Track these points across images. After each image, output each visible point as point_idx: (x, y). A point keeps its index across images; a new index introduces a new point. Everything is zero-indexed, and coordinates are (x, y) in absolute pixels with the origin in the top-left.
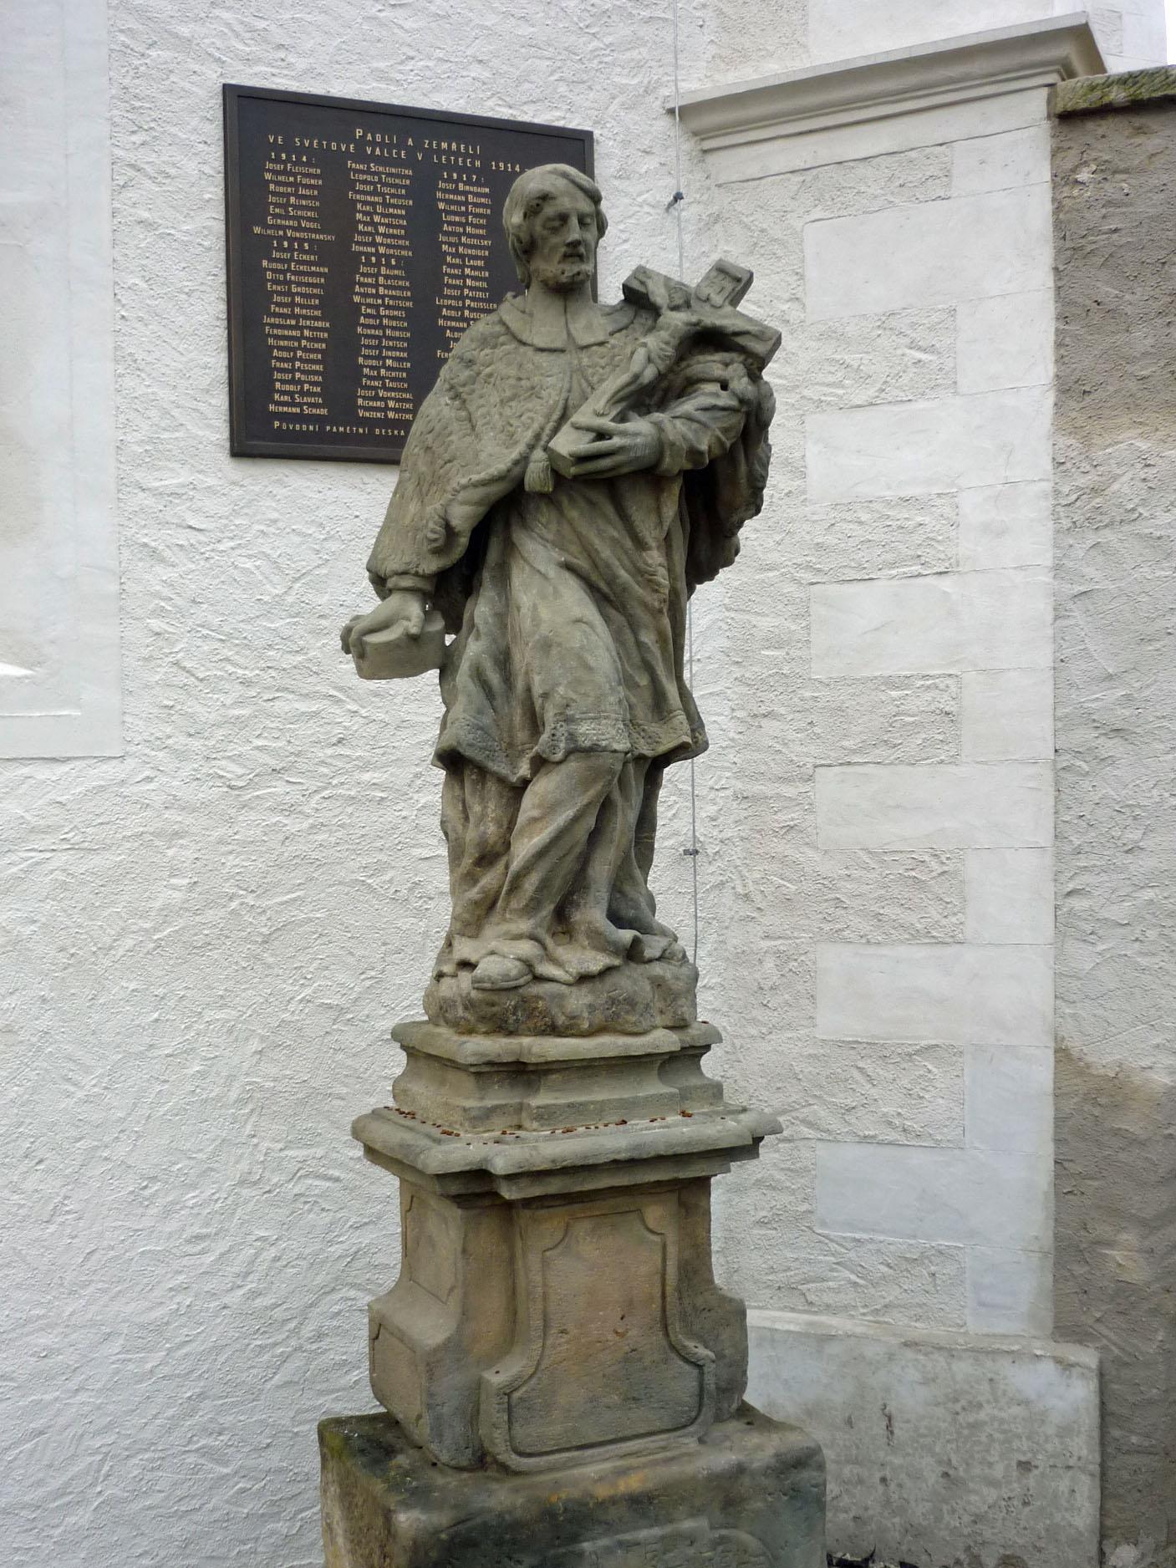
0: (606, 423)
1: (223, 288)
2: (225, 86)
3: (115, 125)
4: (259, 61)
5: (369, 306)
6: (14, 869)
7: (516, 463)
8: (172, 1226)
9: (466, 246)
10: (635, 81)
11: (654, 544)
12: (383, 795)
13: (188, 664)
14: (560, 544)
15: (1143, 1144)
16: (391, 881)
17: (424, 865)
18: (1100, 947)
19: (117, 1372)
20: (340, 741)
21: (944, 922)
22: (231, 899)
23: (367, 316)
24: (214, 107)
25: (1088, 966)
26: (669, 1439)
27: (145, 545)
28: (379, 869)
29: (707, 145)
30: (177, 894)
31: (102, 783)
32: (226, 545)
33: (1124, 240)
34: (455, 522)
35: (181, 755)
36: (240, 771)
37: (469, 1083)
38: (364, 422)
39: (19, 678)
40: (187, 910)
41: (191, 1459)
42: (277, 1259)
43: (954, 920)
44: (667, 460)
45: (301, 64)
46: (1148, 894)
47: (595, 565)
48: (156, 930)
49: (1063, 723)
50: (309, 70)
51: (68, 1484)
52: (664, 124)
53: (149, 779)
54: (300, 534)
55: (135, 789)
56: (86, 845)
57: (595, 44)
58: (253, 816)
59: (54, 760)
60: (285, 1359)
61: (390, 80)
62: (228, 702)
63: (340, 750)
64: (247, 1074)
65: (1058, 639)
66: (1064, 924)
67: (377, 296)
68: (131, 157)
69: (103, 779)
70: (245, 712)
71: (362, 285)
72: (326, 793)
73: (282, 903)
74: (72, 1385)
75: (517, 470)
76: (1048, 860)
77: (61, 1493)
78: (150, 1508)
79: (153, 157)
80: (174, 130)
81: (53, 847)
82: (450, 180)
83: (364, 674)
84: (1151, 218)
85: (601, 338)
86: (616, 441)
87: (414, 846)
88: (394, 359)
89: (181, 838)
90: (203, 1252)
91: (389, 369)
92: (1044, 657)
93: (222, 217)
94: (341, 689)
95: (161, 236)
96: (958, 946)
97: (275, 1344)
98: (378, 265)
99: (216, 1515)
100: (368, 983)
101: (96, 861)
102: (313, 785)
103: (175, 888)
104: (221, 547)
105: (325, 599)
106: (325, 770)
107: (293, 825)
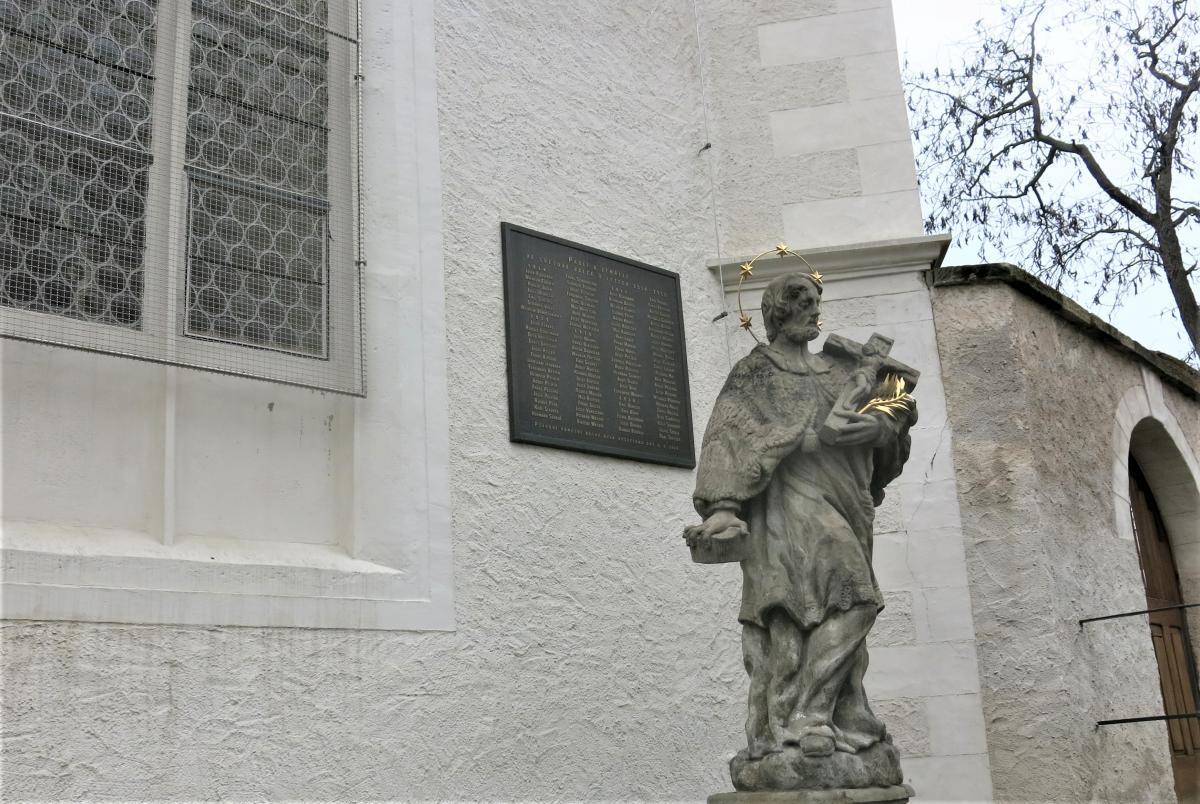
2: (502, 223)
3: (446, 237)
4: (518, 212)
6: (393, 708)
7: (799, 435)
10: (693, 250)
13: (490, 571)
17: (620, 711)
21: (917, 743)
24: (497, 232)
25: (1011, 765)
27: (466, 493)
28: (597, 712)
29: (728, 289)
30: (488, 728)
31: (445, 649)
32: (509, 496)
33: (980, 352)
35: (488, 632)
36: (521, 644)
39: (395, 575)
40: (493, 739)
43: (923, 741)
44: (882, 437)
45: (539, 217)
46: (1043, 719)
47: (840, 497)
49: (978, 619)
50: (543, 221)
52: (707, 275)
53: (470, 648)
54: (548, 493)
55: (463, 654)
56: (434, 692)
57: (674, 227)
59: (416, 632)
61: (581, 233)
62: (514, 598)
63: (573, 633)
65: (971, 568)
68: (455, 258)
69: (444, 646)
72: (566, 661)
73: (547, 735)
75: (799, 439)
76: (978, 700)
79: (466, 258)
80: (476, 245)
82: (615, 291)
83: (696, 559)
84: (996, 341)
87: (615, 698)
88: (593, 391)
89: (489, 688)
92: (962, 580)
93: (502, 297)
95: (471, 305)
96: (927, 759)
100: (594, 792)
101: (440, 703)
102: (560, 655)
103: (487, 724)
104: (506, 497)
105: (562, 535)
107: (552, 681)
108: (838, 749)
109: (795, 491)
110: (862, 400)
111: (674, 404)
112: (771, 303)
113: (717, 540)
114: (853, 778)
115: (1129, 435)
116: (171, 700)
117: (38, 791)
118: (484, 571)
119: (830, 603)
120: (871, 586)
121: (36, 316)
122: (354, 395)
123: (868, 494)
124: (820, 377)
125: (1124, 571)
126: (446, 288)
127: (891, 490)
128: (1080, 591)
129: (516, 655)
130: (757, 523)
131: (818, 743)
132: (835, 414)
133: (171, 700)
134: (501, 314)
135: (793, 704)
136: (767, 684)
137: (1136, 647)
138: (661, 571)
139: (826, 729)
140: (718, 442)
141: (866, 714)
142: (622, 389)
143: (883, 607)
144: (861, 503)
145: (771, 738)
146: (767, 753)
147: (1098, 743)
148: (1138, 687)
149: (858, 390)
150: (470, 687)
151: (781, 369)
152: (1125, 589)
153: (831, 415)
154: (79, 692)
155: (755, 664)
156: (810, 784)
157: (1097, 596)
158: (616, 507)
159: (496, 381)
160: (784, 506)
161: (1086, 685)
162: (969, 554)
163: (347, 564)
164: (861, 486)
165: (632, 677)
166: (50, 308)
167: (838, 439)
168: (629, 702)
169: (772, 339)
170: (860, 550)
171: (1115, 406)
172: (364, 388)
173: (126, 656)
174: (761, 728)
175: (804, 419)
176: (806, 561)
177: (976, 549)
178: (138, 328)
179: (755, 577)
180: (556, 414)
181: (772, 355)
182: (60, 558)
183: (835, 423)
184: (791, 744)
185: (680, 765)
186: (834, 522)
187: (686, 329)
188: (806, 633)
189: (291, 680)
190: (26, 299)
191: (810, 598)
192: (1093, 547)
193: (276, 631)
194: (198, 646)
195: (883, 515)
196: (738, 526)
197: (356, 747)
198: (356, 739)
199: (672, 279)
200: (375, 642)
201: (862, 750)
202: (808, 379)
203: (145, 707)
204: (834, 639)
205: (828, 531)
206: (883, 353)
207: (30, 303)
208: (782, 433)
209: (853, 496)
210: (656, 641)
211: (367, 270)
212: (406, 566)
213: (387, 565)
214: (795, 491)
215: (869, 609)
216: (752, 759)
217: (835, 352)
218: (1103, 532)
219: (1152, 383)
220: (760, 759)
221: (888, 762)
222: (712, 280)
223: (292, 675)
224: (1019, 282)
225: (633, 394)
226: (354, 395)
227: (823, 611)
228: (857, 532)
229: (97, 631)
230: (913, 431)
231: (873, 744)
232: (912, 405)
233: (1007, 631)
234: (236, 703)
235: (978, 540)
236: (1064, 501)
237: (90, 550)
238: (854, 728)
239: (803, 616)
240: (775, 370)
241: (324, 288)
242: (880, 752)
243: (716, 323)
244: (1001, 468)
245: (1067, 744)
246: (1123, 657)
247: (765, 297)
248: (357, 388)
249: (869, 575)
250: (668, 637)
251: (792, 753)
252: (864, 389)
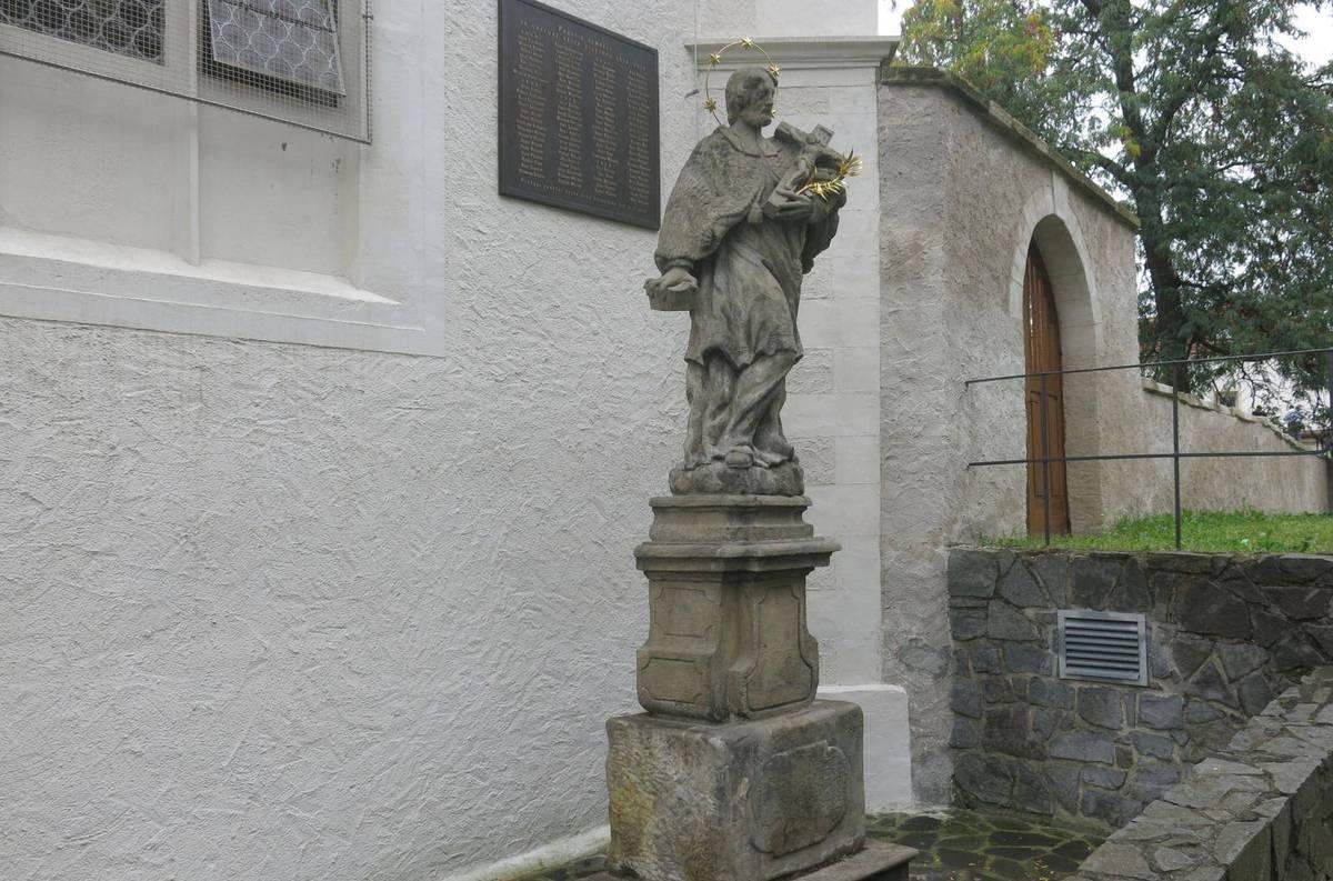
1: (496, 100)
8: (461, 636)
13: (476, 307)
14: (760, 251)
15: (922, 580)
17: (582, 434)
18: (903, 484)
19: (433, 724)
20: (546, 360)
22: (495, 445)
25: (897, 493)
28: (564, 433)
29: (702, 68)
34: (717, 234)
36: (501, 372)
37: (723, 517)
38: (561, 186)
41: (469, 777)
42: (512, 656)
44: (814, 215)
46: (926, 458)
47: (775, 264)
48: (460, 459)
49: (885, 375)
51: (407, 795)
52: (684, 53)
53: (458, 372)
54: (530, 243)
58: (506, 398)
60: (515, 715)
63: (546, 365)
64: (500, 547)
65: (883, 333)
66: (885, 475)
70: (505, 339)
72: (540, 389)
74: (411, 733)
77: (403, 800)
78: (449, 808)
79: (464, 20)
83: (653, 307)
85: (775, 153)
86: (798, 203)
90: (477, 652)
92: (875, 341)
93: (496, 60)
94: (547, 332)
97: (511, 707)
99: (481, 812)
101: (431, 416)
103: (469, 436)
106: (539, 376)
107: (526, 405)
108: (755, 464)
109: (739, 255)
110: (800, 183)
111: (645, 172)
112: (733, 90)
113: (672, 292)
114: (765, 486)
115: (1032, 228)
116: (201, 399)
117: (92, 467)
118: (472, 307)
119: (759, 348)
120: (793, 337)
121: (120, 59)
122: (359, 141)
123: (798, 263)
124: (768, 159)
125: (1009, 344)
126: (446, 47)
127: (820, 259)
128: (970, 358)
129: (497, 381)
130: (706, 281)
131: (739, 458)
132: (778, 192)
133: (201, 399)
134: (495, 76)
135: (722, 428)
136: (703, 411)
137: (1011, 408)
139: (746, 448)
140: (679, 209)
141: (780, 439)
142: (600, 154)
143: (802, 356)
144: (792, 269)
145: (703, 454)
146: (698, 465)
147: (967, 481)
148: (1007, 439)
149: (798, 173)
150: (456, 405)
151: (737, 150)
152: (1009, 359)
153: (774, 192)
154: (122, 387)
155: (695, 395)
156: (730, 489)
157: (984, 363)
158: (588, 260)
159: (487, 138)
160: (728, 267)
161: (964, 434)
162: (883, 320)
163: (352, 294)
164: (793, 255)
165: (594, 406)
166: (43, 27)
167: (778, 214)
169: (732, 122)
170: (786, 307)
171: (1024, 203)
172: (370, 136)
173: (164, 359)
174: (696, 447)
175: (752, 194)
176: (743, 313)
177: (890, 316)
178: (160, 62)
179: (701, 325)
180: (644, 200)
181: (730, 137)
182: (101, 270)
183: (777, 200)
184: (718, 458)
185: (630, 481)
186: (769, 282)
187: (661, 101)
188: (737, 372)
189: (304, 389)
190: (123, 45)
191: (743, 344)
192: (986, 322)
193: (291, 346)
194: (226, 356)
195: (808, 281)
196: (689, 281)
197: (359, 448)
198: (359, 442)
199: (651, 55)
200: (376, 361)
201: (773, 466)
202: (760, 161)
203: (178, 403)
204: (760, 377)
205: (762, 291)
207: (24, 20)
208: (733, 205)
209: (786, 262)
210: (615, 377)
211: (372, 24)
212: (403, 298)
213: (386, 296)
214: (739, 255)
215: (792, 356)
216: (687, 470)
217: (784, 138)
218: (997, 310)
219: (1060, 188)
220: (693, 469)
221: (793, 476)
222: (687, 58)
223: (305, 385)
224: (953, 87)
226: (359, 141)
227: (753, 355)
228: (787, 294)
229: (136, 336)
230: (841, 212)
231: (782, 463)
232: (842, 191)
233: (906, 387)
235: (892, 310)
236: (967, 281)
237: (126, 265)
238: (769, 449)
239: (736, 358)
240: (732, 151)
241: (335, 36)
242: (787, 468)
243: (688, 99)
244: (916, 248)
245: (941, 478)
246: (998, 414)
247: (730, 83)
248: (363, 136)
249: (792, 328)
250: (625, 374)
251: (719, 466)
252: (804, 173)
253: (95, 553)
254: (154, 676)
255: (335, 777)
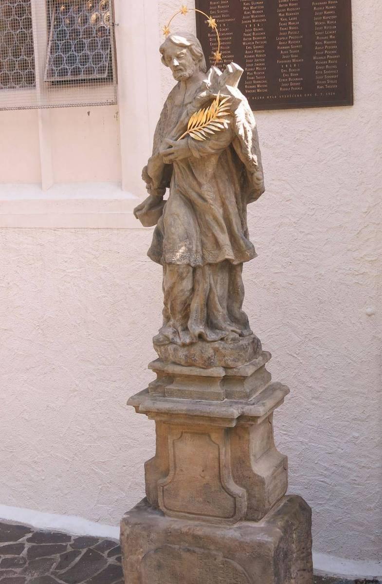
0: (171, 142)
5: (249, 46)
9: (289, 12)
11: (205, 183)
12: (259, 246)
16: (262, 281)
23: (249, 50)
26: (222, 520)
67: (252, 41)
71: (246, 37)
81: (146, 260)
91: (257, 71)
98: (252, 27)
138: (317, 185)
168: (283, 270)
206: (169, 136)
225: (294, 61)
234: (66, 262)
253: (6, 330)
254: (32, 388)
255: (115, 458)
